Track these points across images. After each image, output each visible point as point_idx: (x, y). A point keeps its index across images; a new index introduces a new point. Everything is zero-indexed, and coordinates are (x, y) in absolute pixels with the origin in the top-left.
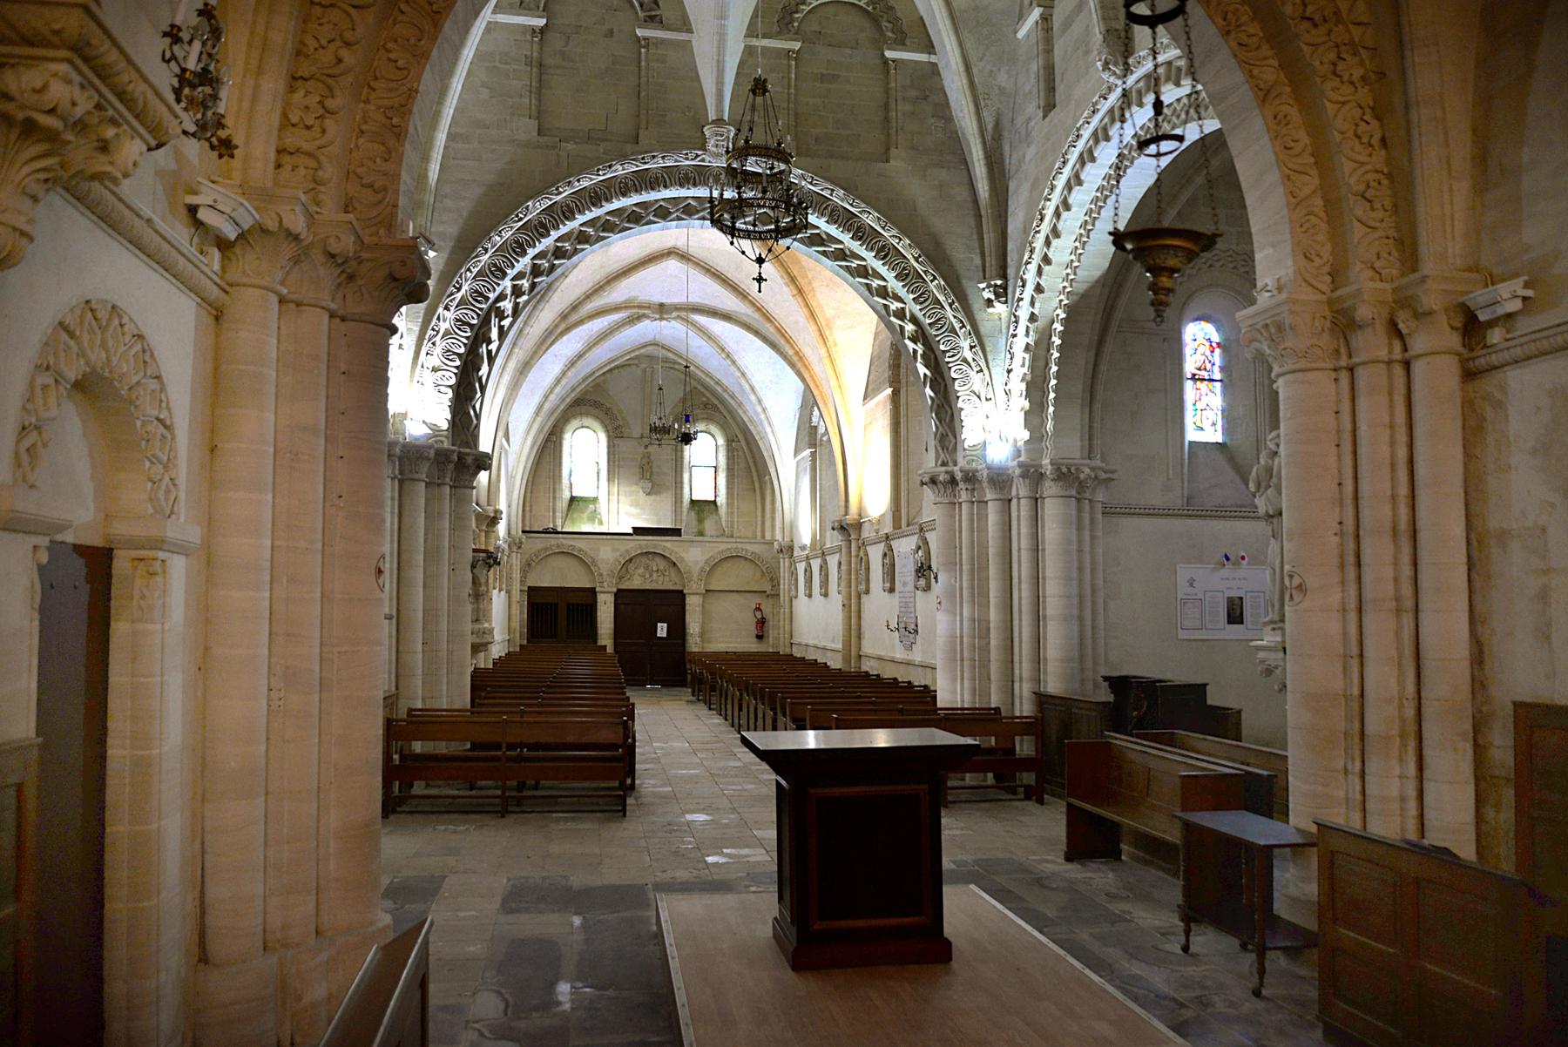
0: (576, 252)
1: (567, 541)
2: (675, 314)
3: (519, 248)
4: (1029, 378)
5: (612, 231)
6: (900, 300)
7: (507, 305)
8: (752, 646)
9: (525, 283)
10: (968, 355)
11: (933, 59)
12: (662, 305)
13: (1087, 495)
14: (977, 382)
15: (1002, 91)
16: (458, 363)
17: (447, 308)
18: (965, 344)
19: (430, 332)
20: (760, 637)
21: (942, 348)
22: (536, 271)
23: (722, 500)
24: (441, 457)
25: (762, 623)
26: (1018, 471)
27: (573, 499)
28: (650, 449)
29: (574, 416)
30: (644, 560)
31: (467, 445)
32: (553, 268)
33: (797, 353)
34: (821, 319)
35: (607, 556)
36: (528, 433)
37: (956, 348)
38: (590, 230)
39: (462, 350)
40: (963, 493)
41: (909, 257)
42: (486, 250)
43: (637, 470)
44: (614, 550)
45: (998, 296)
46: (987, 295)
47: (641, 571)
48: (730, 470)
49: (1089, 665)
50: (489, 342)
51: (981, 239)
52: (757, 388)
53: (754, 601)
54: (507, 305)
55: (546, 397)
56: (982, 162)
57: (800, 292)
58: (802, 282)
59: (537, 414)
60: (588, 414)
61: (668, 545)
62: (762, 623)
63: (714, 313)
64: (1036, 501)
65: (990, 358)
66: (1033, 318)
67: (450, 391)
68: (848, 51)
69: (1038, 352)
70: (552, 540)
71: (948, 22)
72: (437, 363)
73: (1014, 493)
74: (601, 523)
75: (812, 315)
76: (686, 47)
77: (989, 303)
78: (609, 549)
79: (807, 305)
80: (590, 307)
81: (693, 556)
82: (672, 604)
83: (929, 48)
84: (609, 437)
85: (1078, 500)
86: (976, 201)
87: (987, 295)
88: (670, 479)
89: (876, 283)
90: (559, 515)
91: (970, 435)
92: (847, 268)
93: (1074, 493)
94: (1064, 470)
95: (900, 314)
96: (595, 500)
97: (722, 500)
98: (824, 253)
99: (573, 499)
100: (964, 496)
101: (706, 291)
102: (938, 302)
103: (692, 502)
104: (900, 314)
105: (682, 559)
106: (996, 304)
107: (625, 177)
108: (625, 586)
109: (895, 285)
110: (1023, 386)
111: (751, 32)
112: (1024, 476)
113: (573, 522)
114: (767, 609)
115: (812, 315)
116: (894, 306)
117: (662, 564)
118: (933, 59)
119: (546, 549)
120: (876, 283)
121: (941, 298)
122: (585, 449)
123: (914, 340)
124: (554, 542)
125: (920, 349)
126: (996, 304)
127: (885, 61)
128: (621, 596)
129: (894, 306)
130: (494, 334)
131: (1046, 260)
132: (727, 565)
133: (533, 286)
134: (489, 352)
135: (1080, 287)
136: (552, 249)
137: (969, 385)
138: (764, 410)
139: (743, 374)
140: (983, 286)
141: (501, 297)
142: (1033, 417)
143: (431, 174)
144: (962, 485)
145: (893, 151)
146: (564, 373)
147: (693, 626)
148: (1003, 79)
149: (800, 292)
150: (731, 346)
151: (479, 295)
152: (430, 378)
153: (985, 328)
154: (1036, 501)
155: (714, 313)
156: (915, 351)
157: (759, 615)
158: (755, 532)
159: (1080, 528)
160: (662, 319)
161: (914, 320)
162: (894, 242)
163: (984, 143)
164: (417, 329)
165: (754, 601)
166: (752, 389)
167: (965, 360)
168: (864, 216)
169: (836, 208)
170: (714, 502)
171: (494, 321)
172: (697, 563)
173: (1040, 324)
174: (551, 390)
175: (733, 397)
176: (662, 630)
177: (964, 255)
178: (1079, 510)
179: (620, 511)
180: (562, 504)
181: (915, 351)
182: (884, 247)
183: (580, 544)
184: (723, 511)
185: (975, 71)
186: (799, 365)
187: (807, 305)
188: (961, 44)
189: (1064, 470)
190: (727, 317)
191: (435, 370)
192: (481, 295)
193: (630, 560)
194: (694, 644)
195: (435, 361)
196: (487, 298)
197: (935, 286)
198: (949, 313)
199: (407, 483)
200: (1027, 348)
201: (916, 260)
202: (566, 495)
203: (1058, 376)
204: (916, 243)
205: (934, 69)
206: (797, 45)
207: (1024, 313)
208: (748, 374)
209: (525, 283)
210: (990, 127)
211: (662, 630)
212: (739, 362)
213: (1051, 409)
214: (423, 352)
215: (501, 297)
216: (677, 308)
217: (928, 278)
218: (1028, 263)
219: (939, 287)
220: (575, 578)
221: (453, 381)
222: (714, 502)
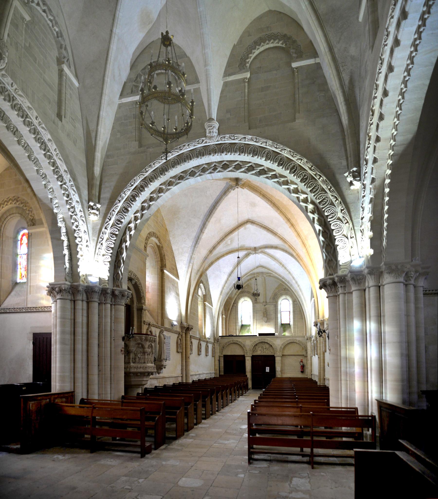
0: (158, 197)
1: (240, 340)
2: (260, 251)
3: (133, 198)
4: (372, 218)
5: (172, 185)
6: (304, 193)
7: (132, 225)
8: (300, 375)
9: (139, 215)
10: (340, 215)
11: (318, 60)
12: (255, 248)
13: (412, 282)
14: (346, 228)
15: (353, 58)
16: (111, 251)
17: (106, 228)
18: (339, 209)
19: (100, 239)
20: (302, 372)
21: (326, 214)
22: (143, 208)
23: (292, 323)
24: (104, 292)
25: (303, 367)
26: (366, 271)
27: (242, 326)
28: (266, 306)
29: (241, 297)
30: (261, 345)
31: (118, 286)
32: (149, 206)
33: (297, 255)
34: (303, 236)
35: (248, 343)
36: (218, 301)
37: (334, 213)
38: (164, 187)
39: (113, 246)
40: (340, 289)
41: (307, 168)
42: (120, 201)
43: (262, 314)
44: (251, 341)
45: (354, 177)
46: (350, 179)
47: (260, 348)
48: (294, 312)
49: (415, 383)
50: (126, 242)
51: (345, 144)
52: (295, 277)
53: (300, 358)
54: (132, 225)
55: (223, 288)
56: (343, 104)
57: (292, 225)
58: (293, 221)
59: (221, 294)
60: (246, 296)
61: (269, 339)
62: (303, 367)
63: (272, 247)
64: (379, 288)
65: (353, 215)
66: (373, 180)
67: (108, 263)
68: (275, 72)
69: (377, 203)
70: (231, 339)
71: (316, 23)
72: (105, 253)
73: (367, 284)
74: (251, 333)
75: (299, 235)
76: (197, 91)
77: (351, 183)
78: (249, 341)
79: (296, 231)
80: (221, 249)
81: (278, 343)
82: (270, 360)
83: (315, 54)
84: (253, 303)
85: (406, 285)
86: (343, 130)
87: (350, 179)
88: (273, 316)
89: (292, 187)
90: (237, 331)
91: (343, 258)
92: (278, 182)
93: (402, 279)
94: (393, 267)
95: (296, 191)
96: (249, 325)
97: (292, 323)
98: (267, 178)
99: (242, 326)
100: (340, 291)
101: (266, 238)
102: (323, 190)
103: (282, 324)
104: (306, 201)
105: (274, 344)
106: (354, 182)
107: (174, 158)
108: (255, 354)
109: (302, 186)
110: (369, 224)
111: (227, 73)
112: (370, 273)
113: (242, 333)
114: (304, 361)
115: (299, 235)
116: (302, 197)
117: (267, 346)
118: (318, 60)
119: (229, 342)
120: (292, 187)
121: (324, 187)
122: (245, 307)
123: (313, 213)
124: (231, 339)
125: (316, 216)
126: (354, 182)
127: (292, 69)
128: (254, 358)
129: (302, 197)
130: (128, 239)
131: (378, 139)
132: (290, 346)
133: (142, 215)
134: (126, 246)
135: (400, 149)
136: (149, 198)
137: (341, 231)
138: (298, 286)
139: (289, 272)
140: (346, 174)
141: (130, 223)
142: (375, 242)
143: (95, 172)
144: (339, 285)
145: (297, 115)
146: (228, 279)
147: (278, 368)
148: (353, 51)
149: (292, 225)
150: (284, 262)
151: (119, 221)
152: (101, 258)
153: (349, 199)
154: (379, 288)
155: (272, 247)
156: (314, 218)
157: (302, 364)
158: (303, 334)
159: (407, 301)
160: (256, 253)
161: (313, 203)
162: (299, 162)
163: (344, 92)
164: (96, 239)
165: (300, 358)
166: (293, 278)
167: (339, 219)
168: (282, 153)
169: (269, 152)
170: (289, 324)
171: (128, 232)
172: (279, 345)
173: (377, 183)
174: (224, 285)
175: (289, 282)
176: (268, 369)
177: (336, 160)
178: (407, 291)
179: (256, 329)
180: (239, 327)
181: (314, 218)
182: (294, 166)
183: (240, 340)
184: (292, 327)
185: (336, 50)
186: (298, 259)
187: (296, 231)
188: (325, 36)
189: (393, 267)
190: (276, 248)
191: (103, 255)
192: (119, 221)
193: (256, 345)
194: (279, 375)
195: (103, 251)
196: (122, 222)
197: (321, 181)
198: (329, 194)
199: (90, 303)
200: (371, 201)
201: (310, 169)
202: (240, 324)
203: (388, 212)
204: (310, 160)
205: (318, 66)
206: (248, 75)
207: (367, 182)
208: (291, 272)
209: (139, 215)
210: (347, 82)
211: (268, 369)
212: (288, 268)
213: (385, 233)
214: (97, 248)
215: (130, 223)
216: (260, 248)
217: (317, 178)
218: (368, 147)
219: (323, 181)
220: (238, 352)
221: (110, 259)
222: (289, 324)
